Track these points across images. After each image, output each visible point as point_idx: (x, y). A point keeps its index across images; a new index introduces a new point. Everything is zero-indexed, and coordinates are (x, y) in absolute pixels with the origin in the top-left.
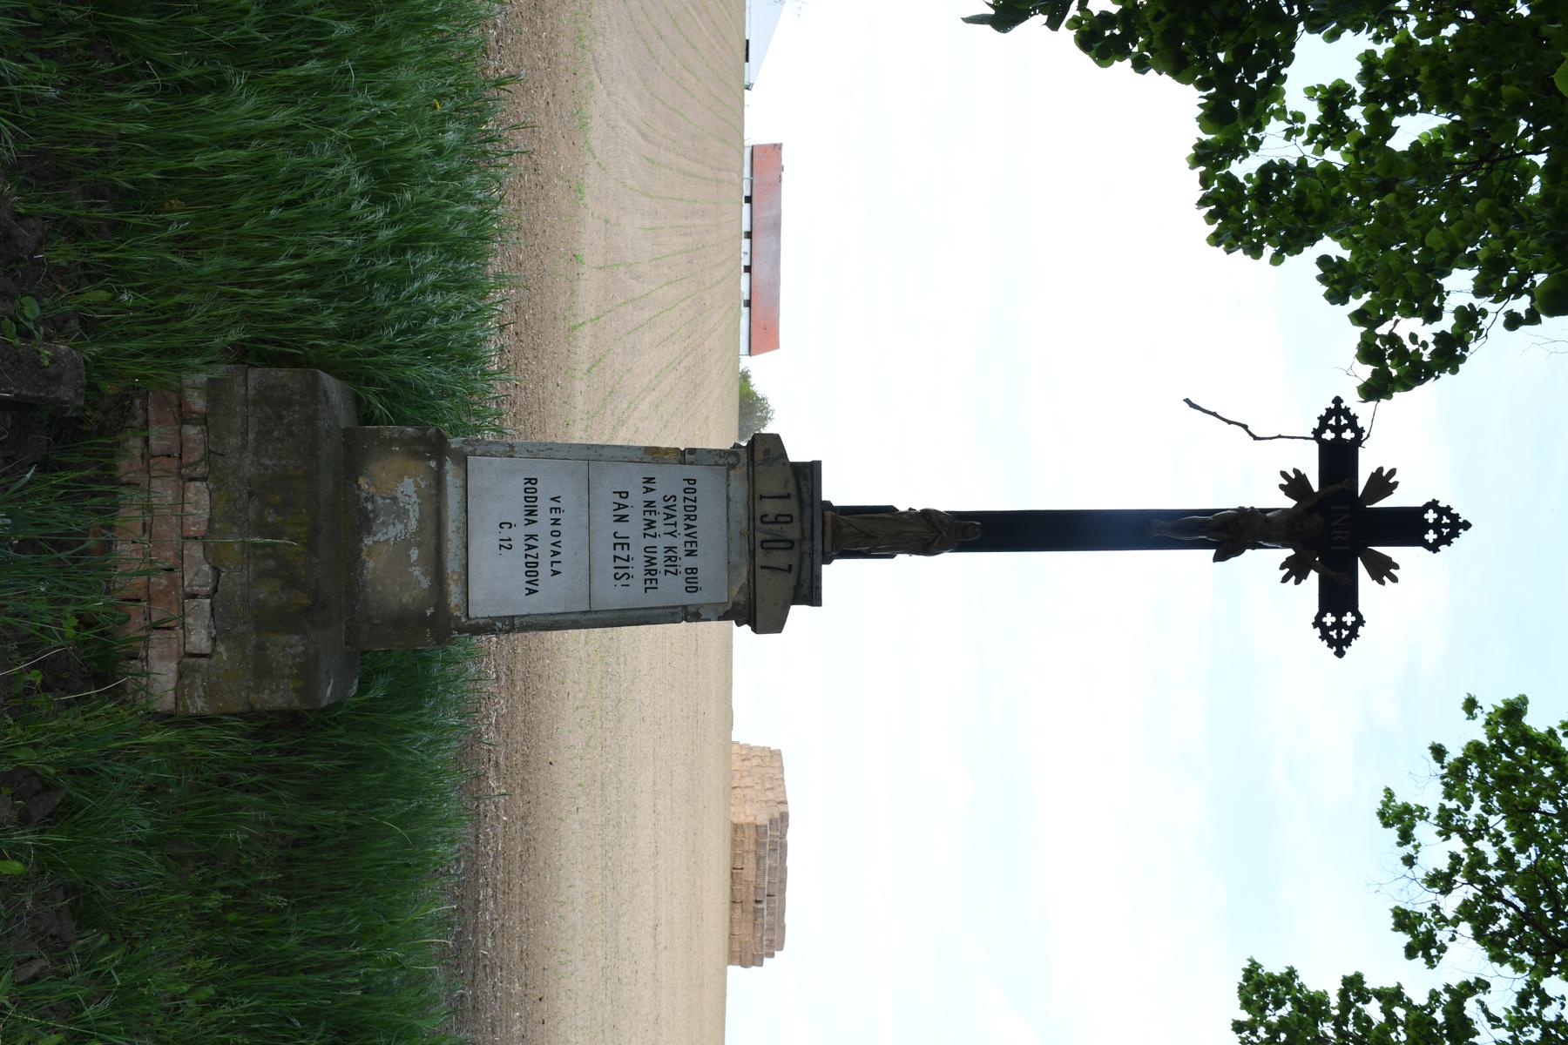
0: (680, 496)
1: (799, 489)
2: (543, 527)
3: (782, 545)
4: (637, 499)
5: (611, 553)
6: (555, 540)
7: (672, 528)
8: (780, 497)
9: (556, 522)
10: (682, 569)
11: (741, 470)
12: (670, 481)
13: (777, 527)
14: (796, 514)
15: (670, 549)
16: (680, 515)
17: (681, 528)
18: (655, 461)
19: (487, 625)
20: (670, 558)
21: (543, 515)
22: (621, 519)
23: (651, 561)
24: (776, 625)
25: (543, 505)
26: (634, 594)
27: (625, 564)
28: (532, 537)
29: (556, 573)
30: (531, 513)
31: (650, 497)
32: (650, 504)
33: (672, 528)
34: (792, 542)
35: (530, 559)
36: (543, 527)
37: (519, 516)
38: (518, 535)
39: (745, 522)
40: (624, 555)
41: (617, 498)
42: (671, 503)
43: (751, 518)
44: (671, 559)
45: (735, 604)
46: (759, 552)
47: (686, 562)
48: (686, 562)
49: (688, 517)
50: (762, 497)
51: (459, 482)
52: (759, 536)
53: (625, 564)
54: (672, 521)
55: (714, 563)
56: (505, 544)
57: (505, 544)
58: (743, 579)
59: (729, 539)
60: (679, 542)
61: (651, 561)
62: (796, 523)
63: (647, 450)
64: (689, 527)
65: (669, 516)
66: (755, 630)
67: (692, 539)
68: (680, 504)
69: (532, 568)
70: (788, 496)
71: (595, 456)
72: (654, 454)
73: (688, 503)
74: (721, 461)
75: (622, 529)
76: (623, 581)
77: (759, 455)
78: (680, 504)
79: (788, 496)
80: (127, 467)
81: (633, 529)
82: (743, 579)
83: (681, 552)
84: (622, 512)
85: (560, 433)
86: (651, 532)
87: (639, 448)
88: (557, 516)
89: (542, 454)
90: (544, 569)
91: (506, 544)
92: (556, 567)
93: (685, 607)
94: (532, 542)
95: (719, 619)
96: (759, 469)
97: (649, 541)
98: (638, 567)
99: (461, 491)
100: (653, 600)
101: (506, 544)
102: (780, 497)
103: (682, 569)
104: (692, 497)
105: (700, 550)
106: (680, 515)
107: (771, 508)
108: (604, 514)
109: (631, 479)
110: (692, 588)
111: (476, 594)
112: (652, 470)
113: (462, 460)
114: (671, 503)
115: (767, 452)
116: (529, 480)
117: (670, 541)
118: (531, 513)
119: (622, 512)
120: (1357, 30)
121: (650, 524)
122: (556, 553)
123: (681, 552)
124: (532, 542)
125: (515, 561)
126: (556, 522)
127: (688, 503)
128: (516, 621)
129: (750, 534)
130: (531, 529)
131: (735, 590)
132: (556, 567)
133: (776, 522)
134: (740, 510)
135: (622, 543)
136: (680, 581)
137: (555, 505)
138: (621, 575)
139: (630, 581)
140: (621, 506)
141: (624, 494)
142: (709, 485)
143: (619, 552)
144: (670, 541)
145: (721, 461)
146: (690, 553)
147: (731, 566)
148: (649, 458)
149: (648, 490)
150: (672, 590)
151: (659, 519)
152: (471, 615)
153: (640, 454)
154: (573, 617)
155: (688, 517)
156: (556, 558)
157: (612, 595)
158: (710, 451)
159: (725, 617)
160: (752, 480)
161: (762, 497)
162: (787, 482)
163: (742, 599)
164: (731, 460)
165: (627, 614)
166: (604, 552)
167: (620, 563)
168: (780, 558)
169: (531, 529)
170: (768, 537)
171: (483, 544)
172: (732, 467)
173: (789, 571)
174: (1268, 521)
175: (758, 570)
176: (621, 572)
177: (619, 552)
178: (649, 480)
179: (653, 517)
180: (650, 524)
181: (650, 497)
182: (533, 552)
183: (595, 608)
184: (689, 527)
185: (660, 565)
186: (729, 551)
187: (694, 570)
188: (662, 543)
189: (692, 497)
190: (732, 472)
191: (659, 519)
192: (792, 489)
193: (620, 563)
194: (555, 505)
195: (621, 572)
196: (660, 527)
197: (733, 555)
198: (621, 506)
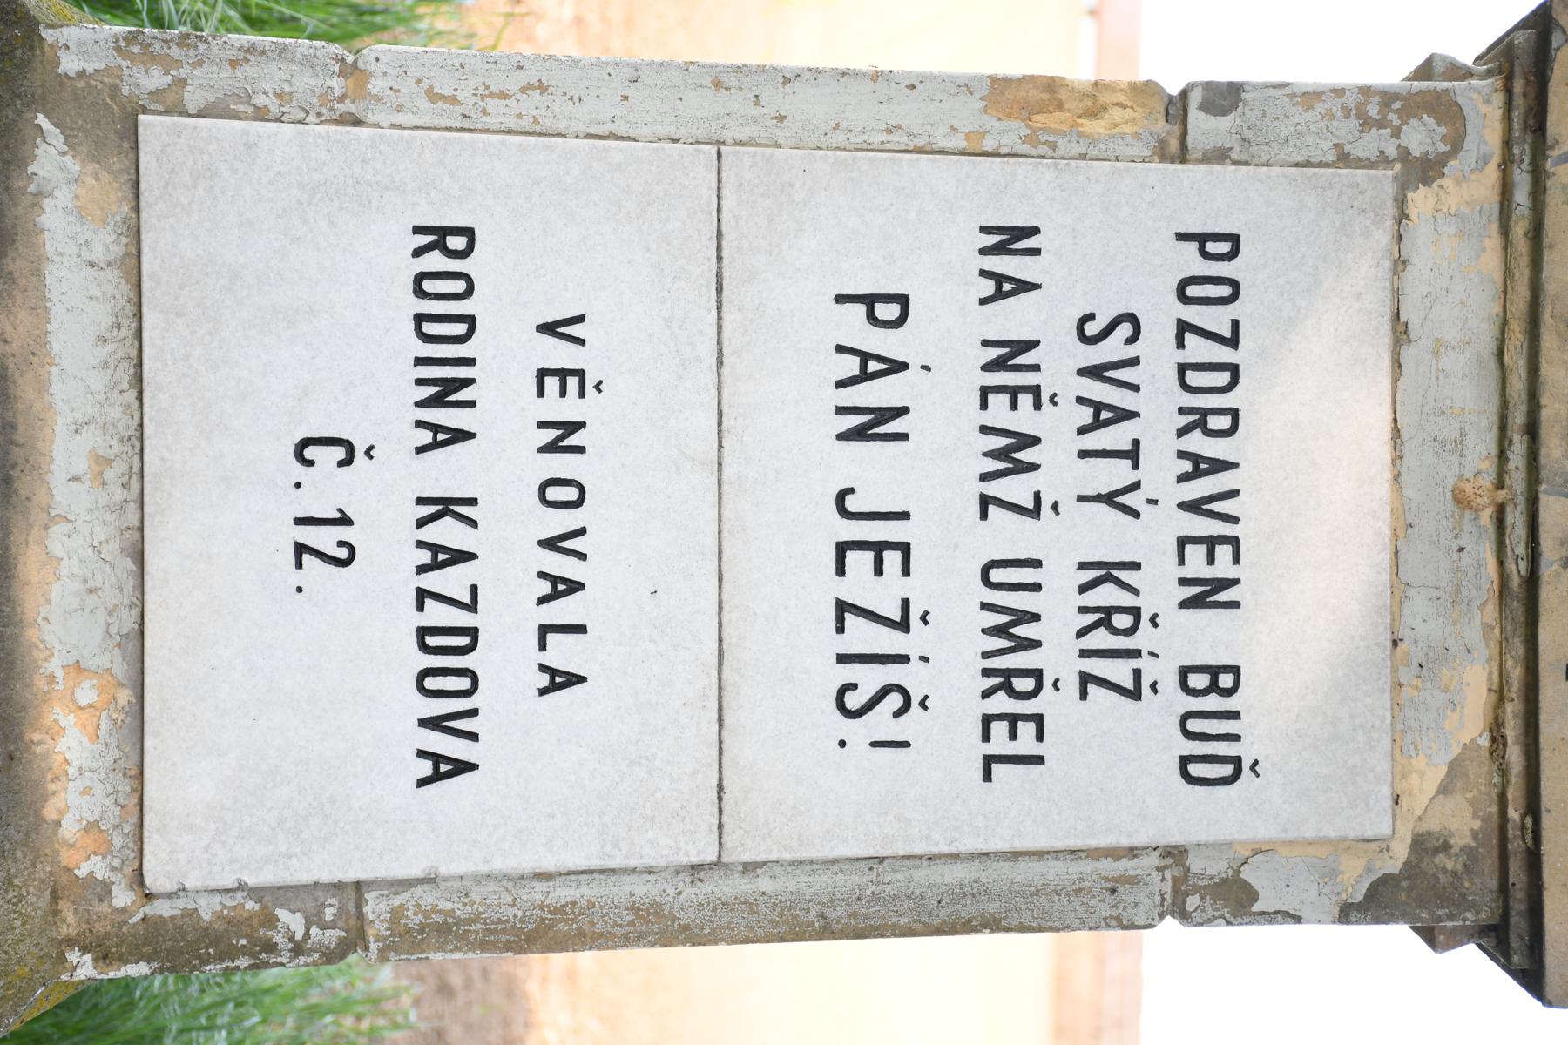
2: (500, 459)
4: (948, 336)
7: (1116, 474)
9: (562, 436)
10: (1162, 671)
11: (1470, 187)
15: (1106, 572)
16: (1157, 407)
17: (1160, 472)
18: (1038, 148)
19: (235, 923)
20: (1105, 617)
21: (505, 406)
22: (874, 425)
23: (1012, 629)
25: (504, 357)
26: (929, 792)
28: (446, 507)
29: (560, 680)
30: (445, 393)
31: (1013, 318)
32: (1010, 353)
33: (1116, 474)
35: (437, 614)
36: (500, 459)
37: (387, 408)
38: (383, 498)
39: (1481, 447)
41: (853, 326)
42: (1114, 348)
45: (1424, 846)
49: (1198, 420)
51: (106, 243)
54: (1116, 437)
56: (324, 544)
57: (324, 544)
59: (1403, 527)
60: (1151, 539)
61: (1012, 629)
63: (1005, 94)
64: (1201, 466)
65: (1103, 416)
67: (1213, 526)
68: (1158, 355)
74: (1370, 144)
75: (876, 473)
76: (881, 722)
78: (1158, 355)
80: (1401, 851)
81: (930, 472)
82: (1470, 726)
83: (1158, 587)
86: (1016, 489)
87: (965, 86)
88: (568, 409)
89: (500, 115)
90: (508, 662)
91: (324, 538)
92: (562, 653)
93: (1175, 854)
94: (447, 532)
95: (1347, 914)
97: (1008, 535)
99: (113, 284)
100: (1019, 813)
101: (324, 538)
103: (1162, 671)
104: (1216, 319)
106: (1157, 407)
108: (794, 399)
110: (1211, 764)
111: (181, 783)
112: (1019, 192)
113: (113, 129)
114: (1114, 348)
116: (437, 237)
117: (1107, 535)
118: (445, 393)
121: (1013, 453)
123: (1158, 587)
124: (447, 532)
126: (562, 436)
127: (1198, 349)
128: (376, 908)
130: (447, 472)
131: (1428, 776)
136: (1155, 725)
137: (560, 354)
138: (872, 695)
140: (875, 367)
141: (886, 307)
143: (860, 583)
144: (1107, 535)
146: (1206, 595)
148: (1009, 133)
149: (1005, 288)
150: (1111, 771)
151: (1056, 429)
152: (155, 878)
153: (968, 115)
154: (641, 889)
155: (1198, 420)
156: (564, 611)
157: (827, 795)
159: (1375, 904)
163: (1462, 821)
164: (1420, 137)
165: (896, 879)
166: (792, 582)
167: (863, 637)
169: (447, 472)
171: (220, 525)
172: (1425, 170)
174: (4, 684)
176: (870, 679)
177: (860, 583)
178: (1010, 239)
179: (1024, 419)
180: (1013, 453)
181: (1013, 318)
182: (452, 581)
183: (743, 849)
184: (1201, 466)
185: (1057, 652)
187: (1220, 678)
188: (1067, 541)
189: (1216, 319)
190: (1421, 200)
191: (1056, 429)
193: (863, 637)
194: (560, 354)
195: (870, 679)
196: (1060, 468)
197: (1419, 604)
198: (875, 367)
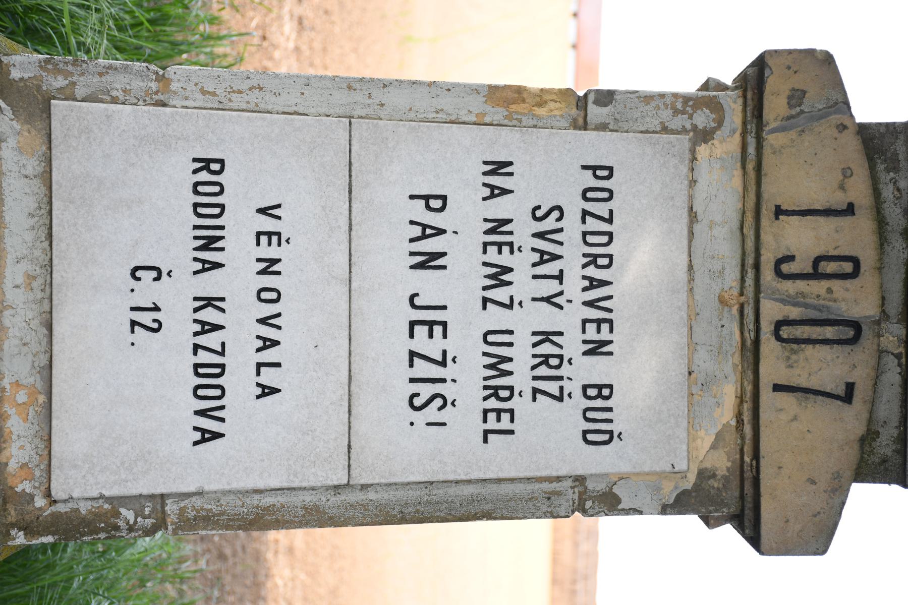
0: (574, 206)
1: (876, 193)
2: (237, 279)
3: (829, 332)
4: (467, 215)
5: (405, 345)
6: (267, 310)
7: (552, 287)
8: (828, 212)
9: (269, 266)
10: (574, 387)
11: (726, 145)
12: (549, 169)
13: (818, 287)
14: (868, 258)
15: (546, 337)
17: (574, 286)
18: (512, 122)
19: (98, 515)
20: (545, 360)
22: (428, 262)
23: (498, 365)
24: (817, 537)
25: (239, 227)
26: (457, 448)
27: (435, 371)
28: (209, 302)
29: (267, 391)
30: (209, 244)
31: (500, 208)
32: (498, 225)
33: (552, 287)
34: (856, 326)
35: (204, 357)
36: (237, 279)
38: (176, 298)
40: (433, 349)
41: (418, 211)
42: (550, 223)
43: (751, 264)
44: (549, 362)
46: (769, 347)
47: (583, 370)
48: (583, 370)
49: (593, 260)
50: (779, 212)
51: (33, 166)
52: (771, 311)
53: (435, 371)
54: (551, 268)
55: (657, 376)
56: (146, 321)
57: (146, 321)
58: (724, 410)
60: (569, 321)
61: (498, 365)
62: (868, 279)
64: (594, 284)
65: (546, 257)
66: (755, 541)
68: (572, 226)
69: (209, 377)
70: (850, 210)
71: (368, 104)
72: (511, 104)
73: (592, 224)
74: (677, 123)
75: (429, 286)
77: (775, 106)
78: (572, 226)
79: (850, 210)
81: (458, 286)
82: (726, 415)
84: (431, 245)
85: (317, 61)
86: (501, 294)
87: (475, 90)
88: (272, 252)
89: (238, 101)
90: (239, 382)
91: (146, 318)
92: (269, 377)
93: (580, 480)
94: (210, 315)
95: (665, 510)
96: (772, 140)
97: (496, 318)
98: (467, 380)
99: (37, 186)
100: (502, 460)
101: (146, 318)
102: (828, 212)
103: (574, 387)
104: (601, 209)
105: (619, 339)
107: (802, 239)
109: (454, 163)
110: (599, 434)
111: (69, 440)
112: (598, 147)
114: (550, 223)
115: (796, 97)
116: (205, 164)
117: (546, 318)
119: (431, 245)
120: (728, 469)
121: (499, 276)
122: (269, 344)
124: (210, 315)
125: (170, 357)
126: (269, 266)
127: (592, 224)
128: (171, 507)
129: (748, 311)
130: (210, 284)
131: (706, 440)
132: (269, 377)
133: (815, 275)
134: (722, 247)
135: (429, 320)
136: (569, 416)
137: (268, 224)
138: (428, 399)
139: (445, 415)
140: (428, 232)
141: (435, 201)
142: (647, 180)
144: (546, 318)
145: (677, 123)
146: (596, 349)
147: (696, 383)
148: (497, 114)
149: (495, 192)
150: (548, 438)
151: (521, 264)
152: (57, 493)
153: (477, 104)
154: (308, 498)
155: (593, 260)
156: (269, 355)
157: (403, 449)
158: (648, 98)
159: (679, 505)
160: (753, 166)
161: (779, 212)
162: (847, 173)
163: (722, 463)
164: (702, 119)
167: (423, 369)
168: (824, 366)
169: (210, 284)
170: (794, 313)
172: (704, 136)
173: (848, 396)
175: (767, 396)
178: (498, 167)
179: (505, 259)
180: (499, 276)
181: (500, 208)
182: (212, 340)
183: (361, 478)
184: (594, 284)
185: (521, 376)
186: (692, 345)
187: (603, 391)
188: (527, 320)
189: (601, 209)
190: (703, 151)
191: (521, 264)
192: (859, 191)
193: (423, 369)
194: (268, 224)
196: (522, 284)
198: (428, 232)
